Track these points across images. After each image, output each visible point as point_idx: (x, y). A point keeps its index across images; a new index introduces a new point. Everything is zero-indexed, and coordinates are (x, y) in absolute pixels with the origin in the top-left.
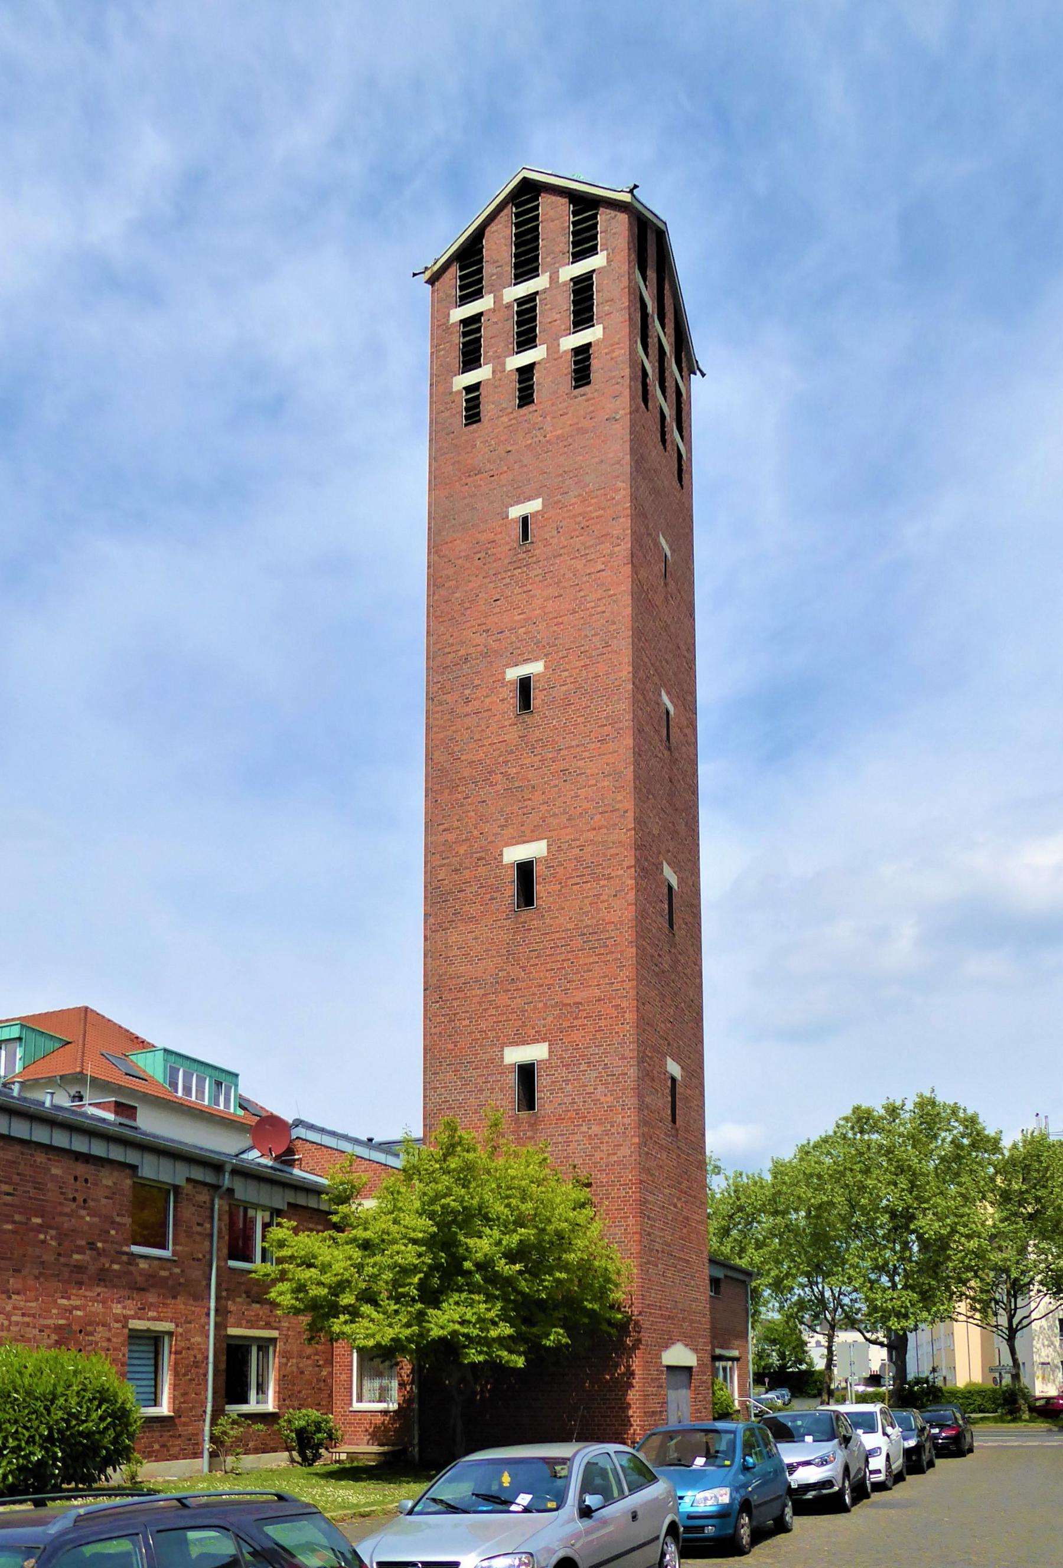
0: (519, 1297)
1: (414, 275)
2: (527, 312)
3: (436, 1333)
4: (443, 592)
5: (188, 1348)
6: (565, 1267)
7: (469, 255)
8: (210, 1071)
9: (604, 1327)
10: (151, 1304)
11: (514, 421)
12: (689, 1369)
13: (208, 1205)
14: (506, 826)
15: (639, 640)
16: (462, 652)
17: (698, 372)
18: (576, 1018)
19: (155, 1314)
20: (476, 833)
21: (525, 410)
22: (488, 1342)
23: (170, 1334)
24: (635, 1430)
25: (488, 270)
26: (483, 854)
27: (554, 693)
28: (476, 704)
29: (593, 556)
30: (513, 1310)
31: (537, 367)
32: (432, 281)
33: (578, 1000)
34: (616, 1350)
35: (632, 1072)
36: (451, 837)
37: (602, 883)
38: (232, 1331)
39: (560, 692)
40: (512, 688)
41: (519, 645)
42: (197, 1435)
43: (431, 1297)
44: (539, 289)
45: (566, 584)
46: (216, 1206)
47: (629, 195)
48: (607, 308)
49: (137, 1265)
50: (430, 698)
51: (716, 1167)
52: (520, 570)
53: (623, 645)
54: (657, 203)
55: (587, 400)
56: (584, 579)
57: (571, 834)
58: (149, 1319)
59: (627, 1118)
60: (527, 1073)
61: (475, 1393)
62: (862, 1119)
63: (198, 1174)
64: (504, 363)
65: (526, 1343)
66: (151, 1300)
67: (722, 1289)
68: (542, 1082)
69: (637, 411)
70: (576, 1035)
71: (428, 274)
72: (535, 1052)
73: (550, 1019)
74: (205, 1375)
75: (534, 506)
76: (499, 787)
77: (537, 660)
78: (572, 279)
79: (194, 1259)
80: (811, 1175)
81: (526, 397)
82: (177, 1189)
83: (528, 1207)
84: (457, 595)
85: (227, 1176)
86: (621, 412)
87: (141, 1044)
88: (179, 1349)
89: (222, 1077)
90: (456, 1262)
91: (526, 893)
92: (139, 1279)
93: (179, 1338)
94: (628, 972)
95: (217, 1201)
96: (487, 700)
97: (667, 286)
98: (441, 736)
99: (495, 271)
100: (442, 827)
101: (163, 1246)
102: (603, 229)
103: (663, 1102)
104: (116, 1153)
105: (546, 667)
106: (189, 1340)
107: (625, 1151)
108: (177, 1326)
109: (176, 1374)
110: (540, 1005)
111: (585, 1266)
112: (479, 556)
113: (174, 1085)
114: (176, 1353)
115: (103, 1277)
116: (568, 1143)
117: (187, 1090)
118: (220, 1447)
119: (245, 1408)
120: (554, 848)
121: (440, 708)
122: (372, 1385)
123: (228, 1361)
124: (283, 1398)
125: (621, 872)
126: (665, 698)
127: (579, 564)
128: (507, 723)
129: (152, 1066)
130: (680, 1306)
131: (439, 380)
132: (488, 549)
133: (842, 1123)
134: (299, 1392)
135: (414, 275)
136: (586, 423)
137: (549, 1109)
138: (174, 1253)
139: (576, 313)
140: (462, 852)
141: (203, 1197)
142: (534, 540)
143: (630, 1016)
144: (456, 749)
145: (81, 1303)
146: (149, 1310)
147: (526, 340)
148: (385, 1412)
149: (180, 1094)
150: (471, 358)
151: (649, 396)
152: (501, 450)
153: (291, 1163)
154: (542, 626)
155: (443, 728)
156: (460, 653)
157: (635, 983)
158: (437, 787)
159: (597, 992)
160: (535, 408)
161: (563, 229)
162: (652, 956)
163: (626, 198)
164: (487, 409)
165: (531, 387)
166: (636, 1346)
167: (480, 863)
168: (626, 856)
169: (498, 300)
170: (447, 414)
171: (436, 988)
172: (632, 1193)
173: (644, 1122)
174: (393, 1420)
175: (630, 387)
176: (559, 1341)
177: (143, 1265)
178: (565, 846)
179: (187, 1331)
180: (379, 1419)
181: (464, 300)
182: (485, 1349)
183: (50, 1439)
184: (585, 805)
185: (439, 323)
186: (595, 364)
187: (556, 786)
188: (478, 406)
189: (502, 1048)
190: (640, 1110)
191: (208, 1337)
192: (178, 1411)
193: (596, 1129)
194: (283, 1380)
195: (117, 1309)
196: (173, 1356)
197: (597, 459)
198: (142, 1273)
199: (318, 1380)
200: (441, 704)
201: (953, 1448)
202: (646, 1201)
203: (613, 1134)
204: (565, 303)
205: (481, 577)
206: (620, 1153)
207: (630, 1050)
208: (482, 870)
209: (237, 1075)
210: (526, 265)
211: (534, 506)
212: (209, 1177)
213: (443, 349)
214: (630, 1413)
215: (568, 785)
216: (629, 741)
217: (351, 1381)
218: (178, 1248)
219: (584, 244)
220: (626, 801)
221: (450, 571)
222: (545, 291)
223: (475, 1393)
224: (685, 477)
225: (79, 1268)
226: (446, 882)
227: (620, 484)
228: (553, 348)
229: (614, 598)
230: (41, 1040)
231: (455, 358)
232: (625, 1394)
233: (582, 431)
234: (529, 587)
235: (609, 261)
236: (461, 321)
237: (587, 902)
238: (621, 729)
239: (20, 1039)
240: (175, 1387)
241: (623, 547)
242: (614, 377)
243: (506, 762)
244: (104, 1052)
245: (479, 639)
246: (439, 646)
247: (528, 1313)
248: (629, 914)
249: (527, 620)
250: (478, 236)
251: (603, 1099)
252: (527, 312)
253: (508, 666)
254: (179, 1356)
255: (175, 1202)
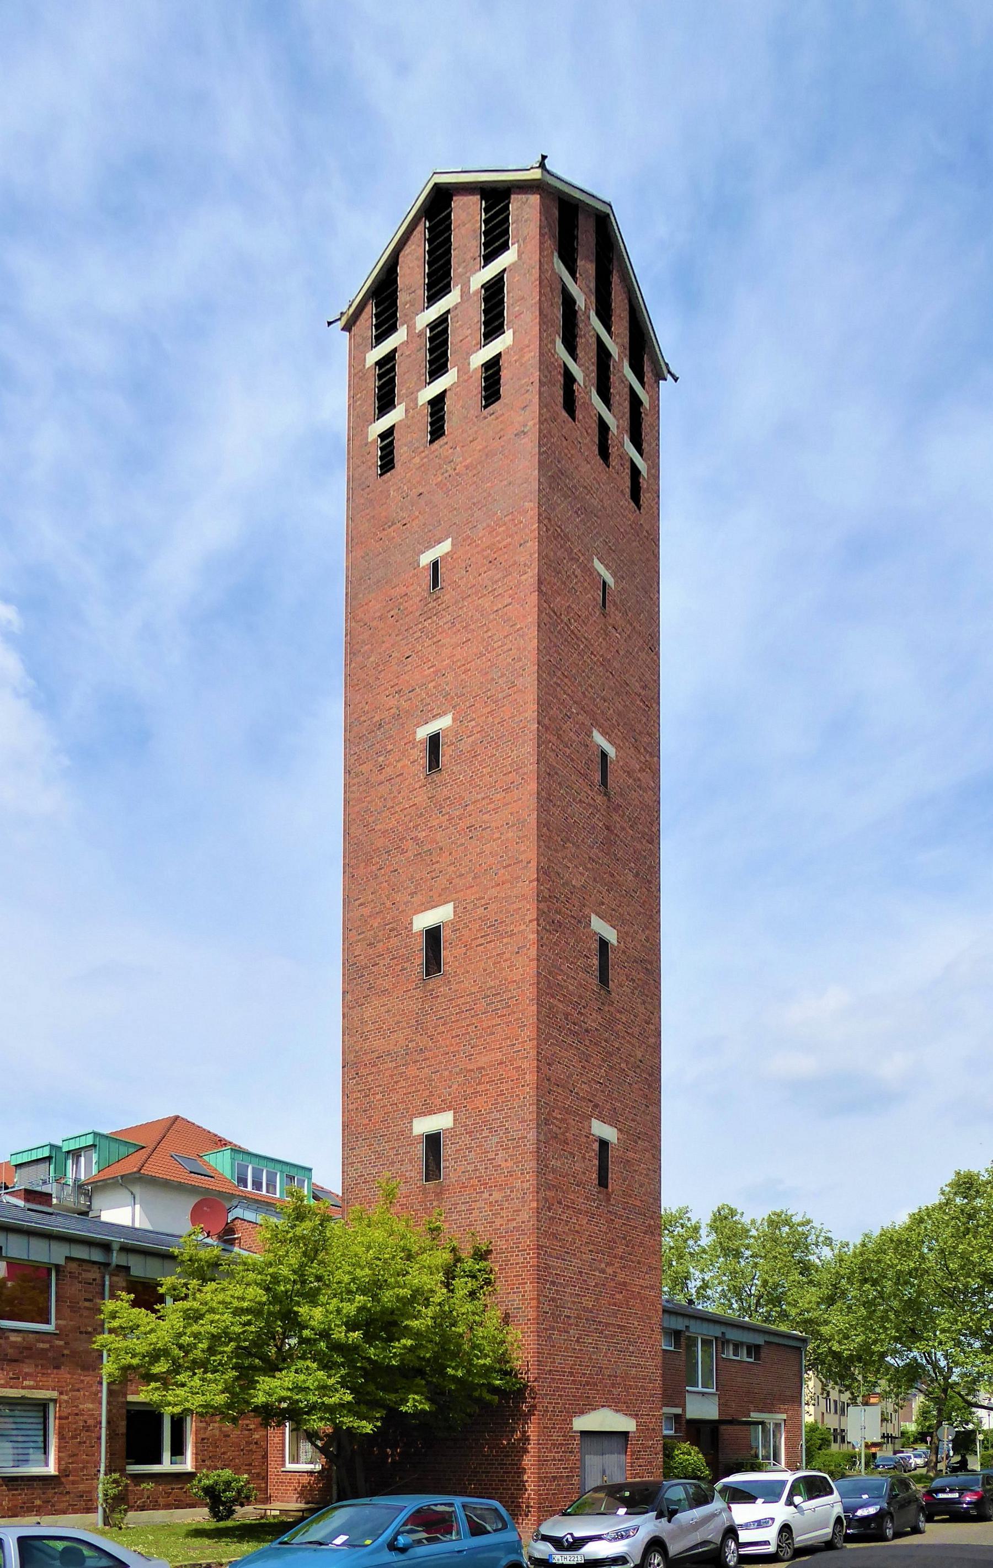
0: (366, 1365)
1: (330, 323)
5: (77, 1414)
8: (279, 1166)
10: (27, 1374)
11: (425, 460)
12: (625, 1434)
13: (98, 1281)
14: (415, 893)
15: (552, 674)
16: (377, 719)
17: (669, 377)
18: (479, 1084)
19: (32, 1383)
20: (388, 904)
21: (436, 444)
23: (55, 1401)
24: (529, 1494)
25: (402, 298)
26: (394, 925)
27: (461, 746)
28: (388, 770)
29: (500, 591)
30: (362, 1376)
31: (448, 394)
32: (347, 328)
33: (479, 1064)
34: (512, 1416)
35: (532, 1136)
36: (366, 911)
37: (505, 940)
39: (465, 745)
40: (421, 747)
41: (428, 700)
42: (90, 1492)
44: (451, 306)
45: (472, 627)
46: (107, 1283)
47: (539, 171)
48: (517, 308)
49: (7, 1338)
50: (347, 772)
51: (827, 1238)
52: (430, 621)
53: (529, 682)
54: (578, 171)
55: (497, 418)
56: (491, 617)
57: (476, 893)
58: (23, 1388)
61: (387, 1456)
62: (967, 1185)
63: (80, 1252)
64: (416, 399)
65: (384, 1409)
66: (27, 1370)
67: (763, 1355)
68: (447, 1151)
69: (554, 420)
70: (479, 1102)
71: (344, 319)
72: (441, 1122)
73: (455, 1087)
74: (99, 1438)
75: (445, 547)
76: (410, 854)
77: (445, 713)
78: (482, 286)
79: (81, 1333)
80: (900, 1242)
82: (57, 1267)
84: (371, 659)
85: (115, 1254)
86: (531, 423)
88: (64, 1414)
89: (293, 1172)
91: (433, 961)
92: (10, 1351)
93: (64, 1405)
94: (529, 1032)
95: (107, 1278)
96: (399, 765)
97: (615, 279)
98: (357, 809)
99: (408, 298)
100: (357, 903)
101: (48, 1322)
102: (515, 218)
105: (454, 720)
106: (77, 1407)
107: (524, 1216)
108: (61, 1393)
109: (61, 1437)
110: (447, 1073)
112: (392, 613)
113: (242, 1181)
114: (60, 1418)
116: (470, 1211)
117: (257, 1185)
118: (120, 1502)
119: (155, 1468)
120: (460, 910)
121: (356, 780)
123: (128, 1425)
124: (200, 1460)
125: (523, 927)
126: (599, 739)
127: (486, 603)
128: (417, 786)
130: (607, 1372)
132: (401, 604)
133: (947, 1189)
134: (224, 1453)
135: (330, 323)
137: (453, 1177)
138: (57, 1327)
139: (486, 323)
140: (376, 925)
141: (94, 1274)
142: (444, 584)
143: (531, 1078)
144: (371, 820)
146: (25, 1379)
148: (311, 1473)
149: (250, 1188)
150: (386, 402)
151: (578, 403)
153: (232, 1242)
155: (360, 800)
156: (375, 720)
157: (535, 1042)
158: (353, 862)
160: (445, 440)
161: (474, 231)
162: (567, 1015)
163: (536, 174)
164: (401, 453)
165: (442, 418)
166: (531, 1413)
167: (393, 934)
168: (528, 910)
169: (410, 329)
170: (363, 468)
171: (354, 1065)
174: (318, 1481)
175: (540, 393)
176: (415, 1406)
177: (14, 1338)
178: (470, 907)
179: (74, 1399)
180: (305, 1479)
182: (327, 1415)
186: (505, 375)
187: (462, 844)
188: (392, 452)
189: (411, 1119)
190: (540, 1173)
191: (101, 1403)
192: (64, 1472)
193: (497, 1195)
194: (201, 1442)
196: (57, 1421)
197: (505, 483)
198: (14, 1345)
199: (248, 1443)
200: (357, 776)
201: (973, 1512)
202: (548, 1267)
203: (513, 1199)
205: (394, 635)
206: (519, 1219)
207: (530, 1112)
208: (394, 941)
209: (310, 1170)
210: (438, 284)
212: (97, 1256)
213: (359, 399)
214: (525, 1478)
215: (474, 841)
216: (533, 786)
217: (284, 1444)
218: (60, 1322)
219: (495, 241)
220: (529, 851)
221: (365, 636)
222: (456, 307)
223: (387, 1456)
224: (645, 497)
226: (362, 957)
229: (521, 632)
230: (114, 1146)
231: (371, 404)
232: (520, 1460)
234: (439, 637)
236: (377, 363)
237: (490, 962)
238: (525, 774)
239: (94, 1146)
240: (60, 1449)
241: (530, 574)
242: (522, 386)
243: (416, 827)
244: (173, 1154)
245: (392, 702)
246: (355, 716)
249: (436, 673)
251: (503, 1164)
253: (418, 725)
254: (64, 1421)
255: (57, 1280)
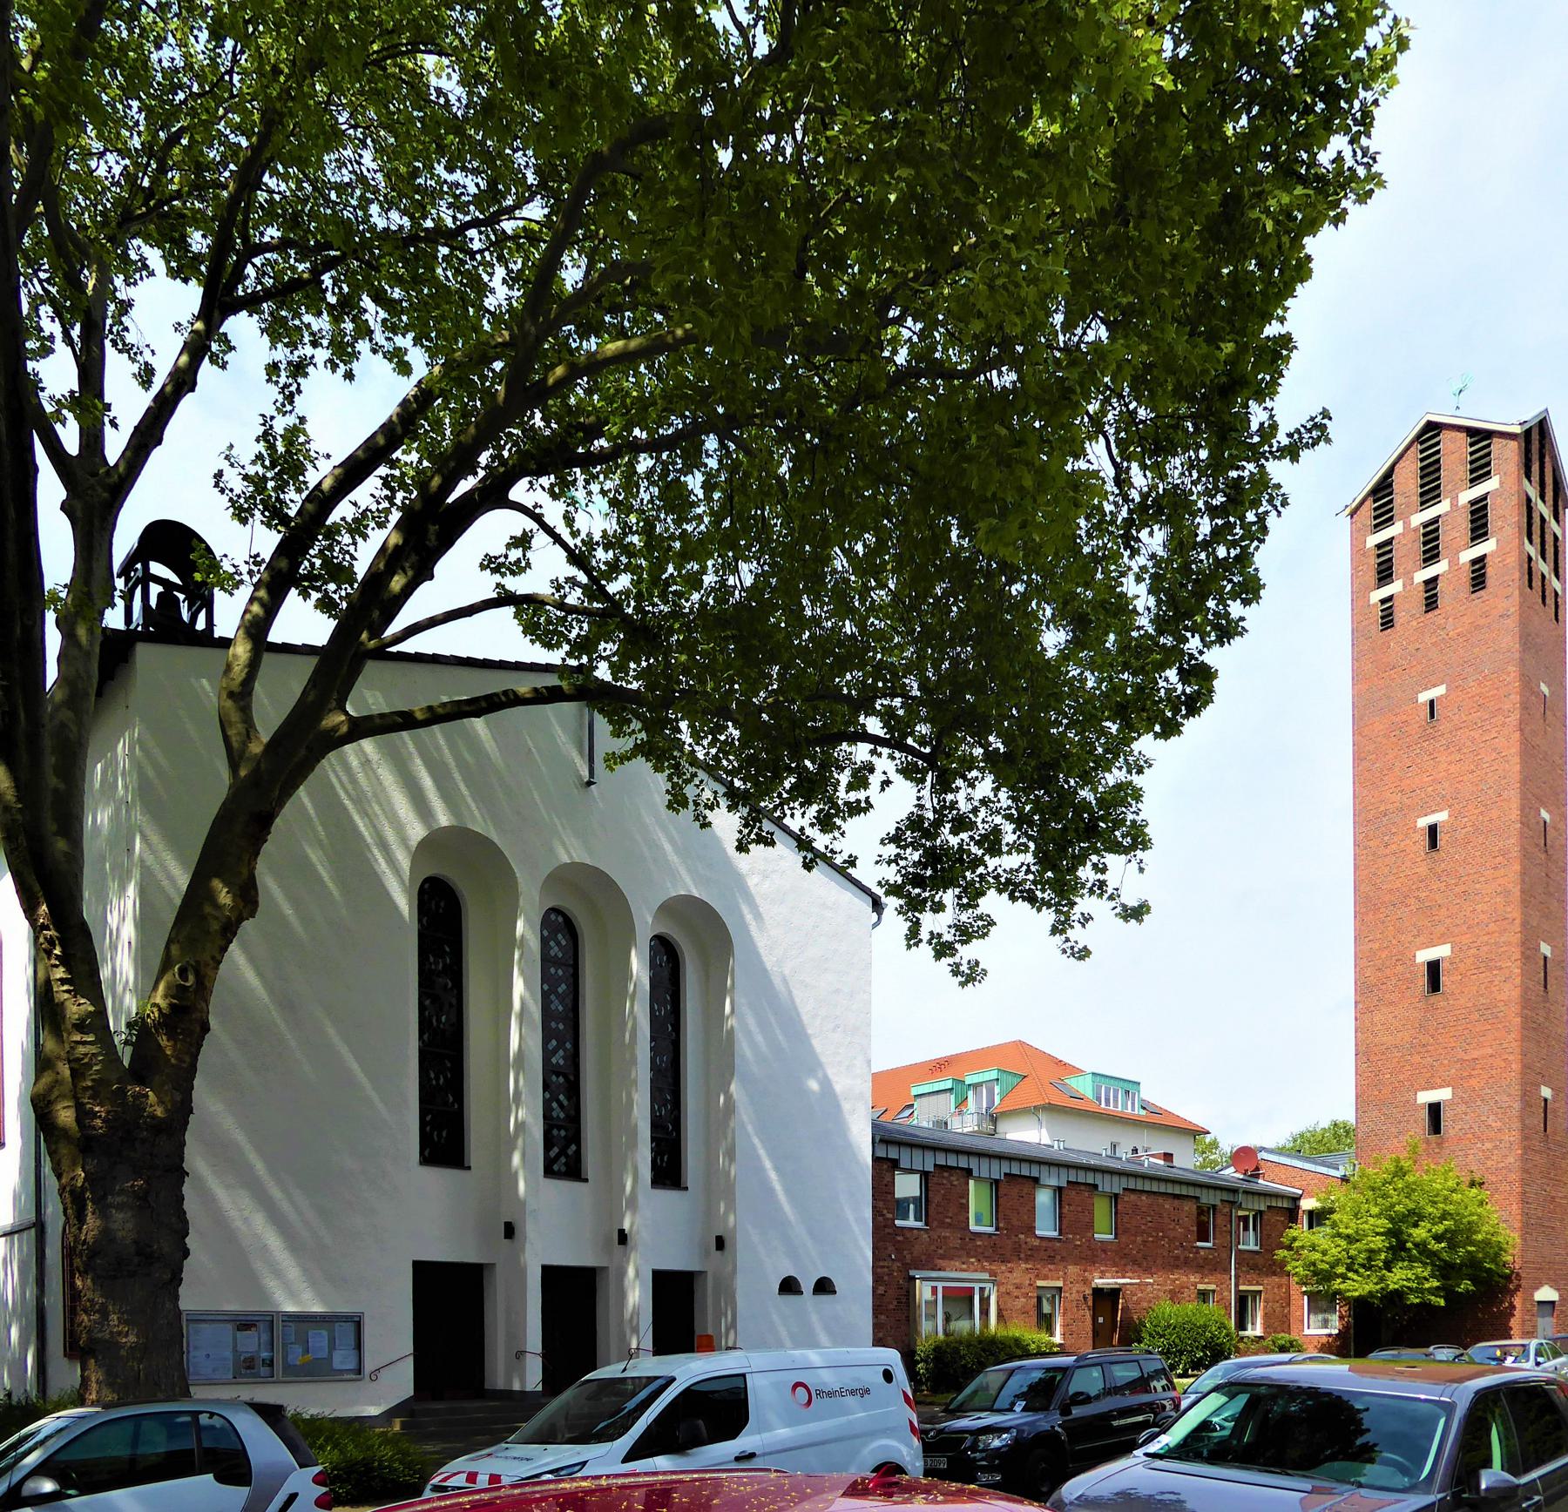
2: (1431, 533)
3: (1392, 1287)
4: (1366, 764)
6: (1472, 1243)
7: (1383, 488)
9: (1496, 1278)
12: (1553, 1303)
22: (1422, 1291)
25: (1398, 500)
27: (1457, 835)
35: (1517, 1105)
36: (1377, 946)
38: (1242, 1288)
39: (1460, 834)
43: (1388, 1266)
59: (1513, 1136)
60: (1435, 1109)
63: (1226, 1196)
68: (1445, 1116)
70: (1473, 1082)
71: (1348, 511)
75: (1438, 692)
81: (1431, 603)
83: (1450, 1208)
87: (1076, 1071)
90: (1401, 1246)
97: (1547, 459)
101: (1207, 1241)
103: (1537, 1120)
104: (1191, 1192)
111: (1487, 1243)
113: (1099, 1099)
115: (1187, 1262)
116: (1466, 1156)
117: (1107, 1102)
122: (1316, 1319)
129: (1083, 1086)
131: (1359, 596)
136: (1482, 621)
137: (1452, 1132)
145: (1179, 1278)
147: (1431, 556)
150: (1385, 574)
152: (1411, 648)
153: (1257, 1176)
154: (1446, 785)
159: (1490, 1051)
164: (1400, 616)
169: (1407, 524)
172: (1517, 1188)
173: (1525, 1138)
180: (1325, 1340)
181: (1378, 527)
183: (1205, 1347)
184: (1482, 916)
185: (1357, 550)
186: (1490, 571)
193: (1488, 1145)
194: (1266, 1316)
195: (1192, 1279)
204: (1464, 524)
207: (1516, 1090)
208: (1400, 968)
211: (1438, 692)
216: (1517, 867)
219: (1480, 471)
220: (1515, 913)
222: (1446, 514)
225: (1177, 1258)
227: (1511, 668)
228: (1454, 562)
231: (1372, 576)
233: (1478, 627)
235: (1501, 483)
247: (1446, 1271)
248: (1516, 993)
250: (1389, 473)
252: (1431, 533)
